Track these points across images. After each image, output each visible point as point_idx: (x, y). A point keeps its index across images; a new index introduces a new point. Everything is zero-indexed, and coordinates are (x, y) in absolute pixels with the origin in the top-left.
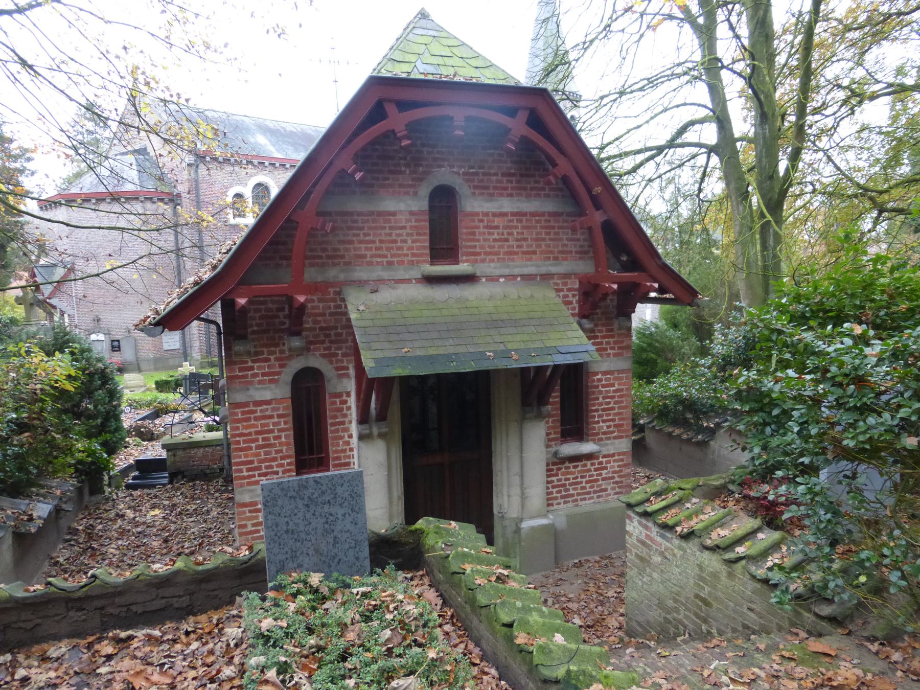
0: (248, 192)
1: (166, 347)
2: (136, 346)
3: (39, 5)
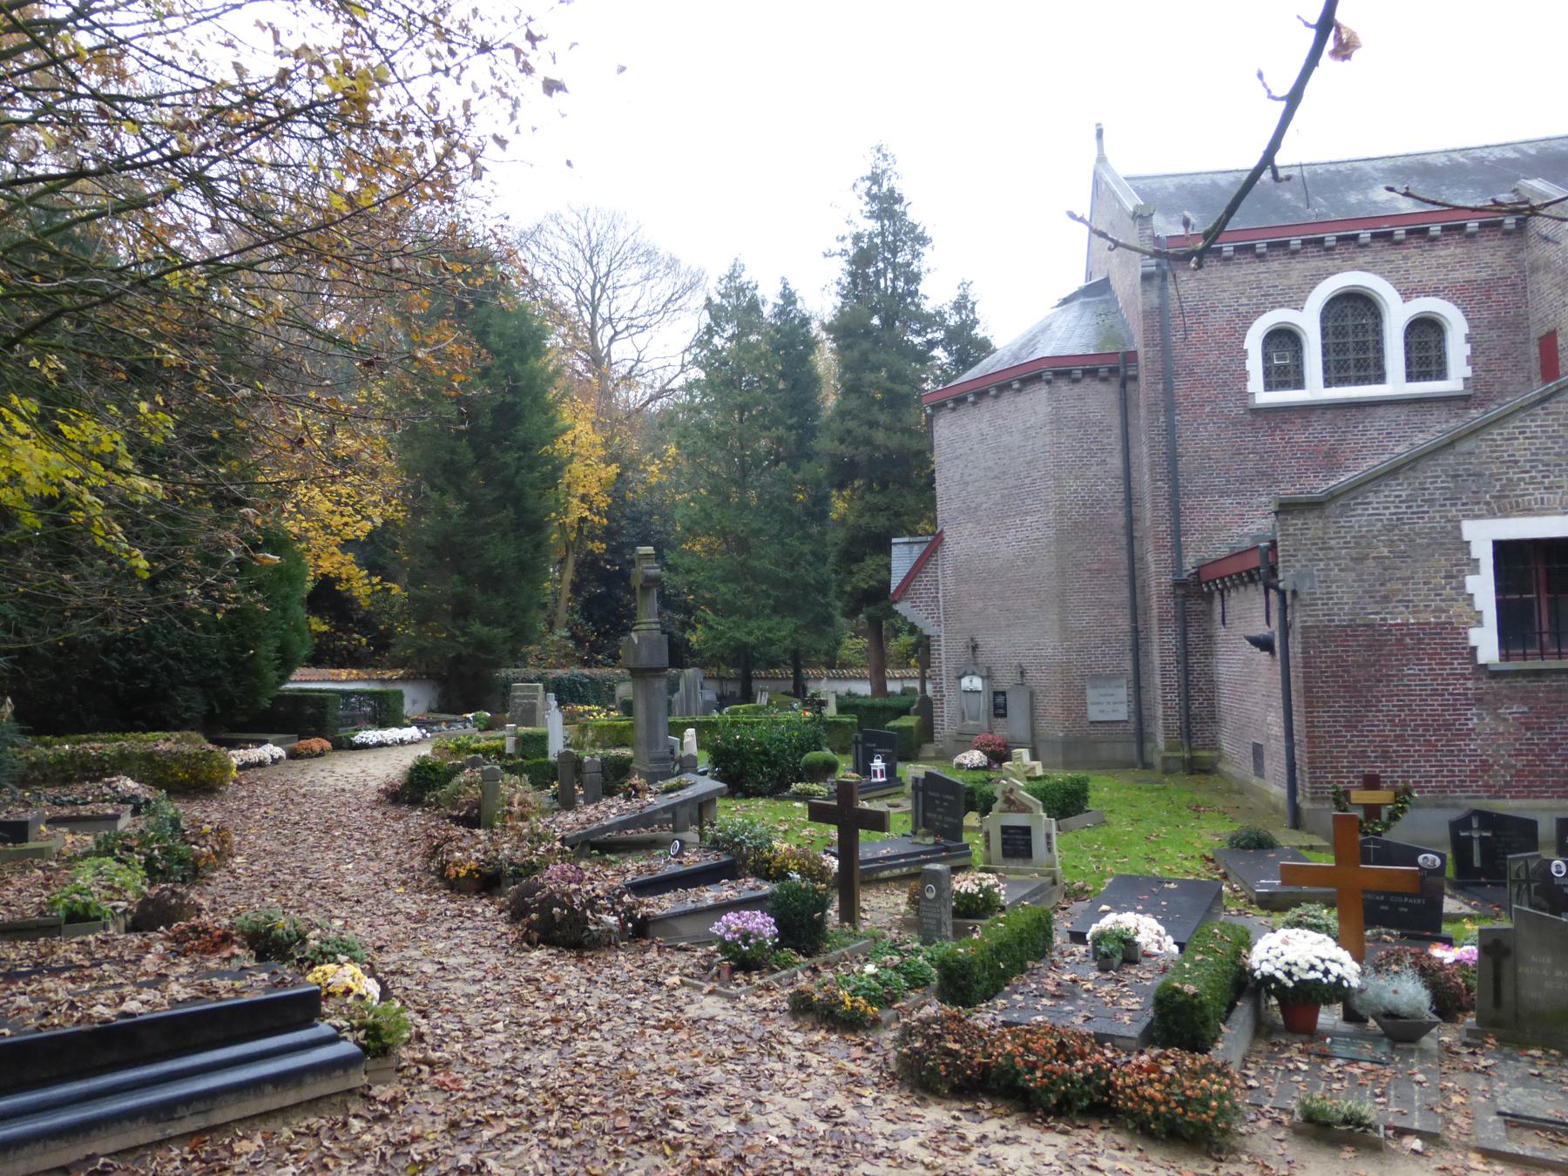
0: (1308, 321)
1: (1094, 714)
2: (1032, 708)
3: (238, 6)
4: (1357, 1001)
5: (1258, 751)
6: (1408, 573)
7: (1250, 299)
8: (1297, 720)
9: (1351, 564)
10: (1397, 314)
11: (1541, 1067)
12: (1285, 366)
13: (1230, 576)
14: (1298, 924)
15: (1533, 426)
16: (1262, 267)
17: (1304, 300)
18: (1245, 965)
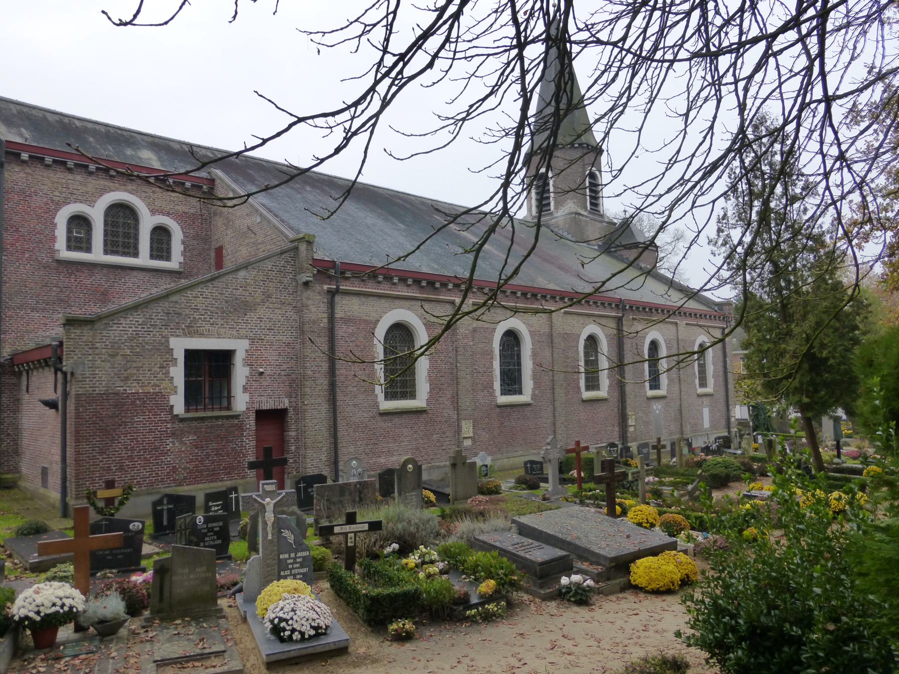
0: (97, 214)
4: (82, 619)
5: (45, 472)
6: (140, 365)
7: (60, 193)
8: (70, 451)
9: (109, 358)
10: (147, 222)
11: (180, 629)
12: (81, 238)
13: (33, 362)
14: (54, 578)
15: (207, 292)
16: (70, 176)
17: (95, 202)
18: (8, 613)
